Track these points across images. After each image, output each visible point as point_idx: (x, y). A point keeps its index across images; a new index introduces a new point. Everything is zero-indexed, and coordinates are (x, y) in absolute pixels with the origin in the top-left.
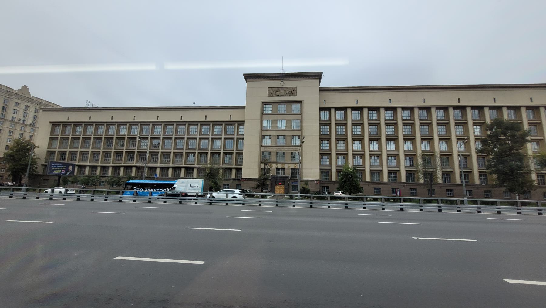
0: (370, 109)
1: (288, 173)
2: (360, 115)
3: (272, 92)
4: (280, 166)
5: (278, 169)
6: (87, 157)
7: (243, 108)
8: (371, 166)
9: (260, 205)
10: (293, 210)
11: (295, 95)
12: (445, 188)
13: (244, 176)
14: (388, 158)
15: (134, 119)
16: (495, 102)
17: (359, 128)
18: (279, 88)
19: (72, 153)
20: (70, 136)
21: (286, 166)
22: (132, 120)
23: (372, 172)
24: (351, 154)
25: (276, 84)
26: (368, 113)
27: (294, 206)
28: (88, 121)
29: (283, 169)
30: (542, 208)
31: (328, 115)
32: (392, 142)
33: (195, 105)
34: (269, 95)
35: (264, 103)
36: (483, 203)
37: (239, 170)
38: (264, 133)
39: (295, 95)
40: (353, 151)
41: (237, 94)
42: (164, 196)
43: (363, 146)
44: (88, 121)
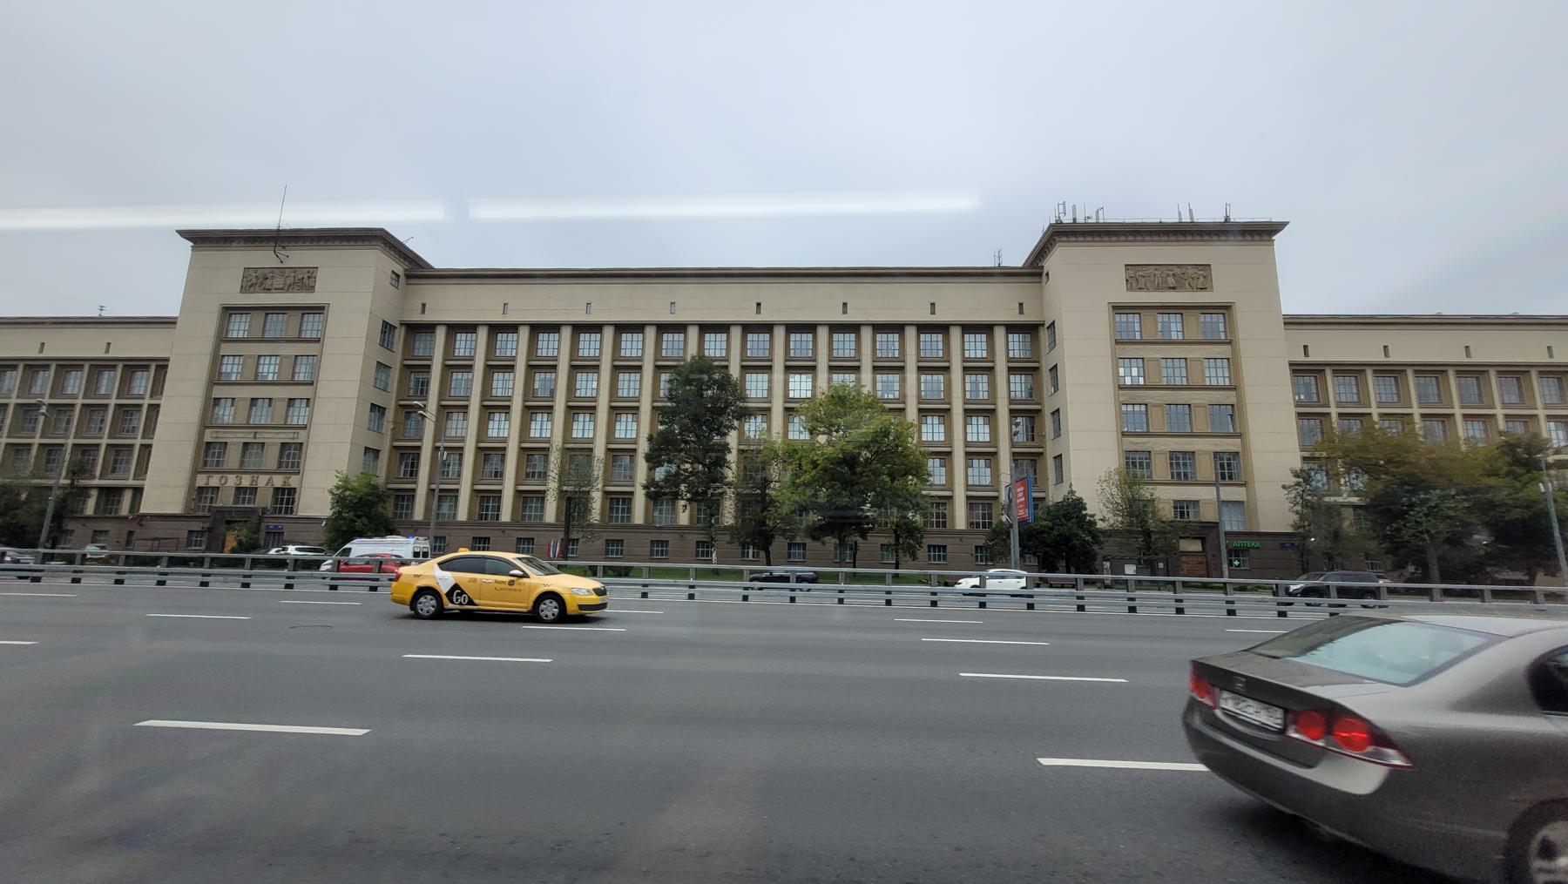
0: (968, 328)
1: (264, 500)
2: (984, 346)
3: (255, 280)
4: (246, 481)
5: (239, 490)
6: (128, 462)
7: (169, 322)
8: (968, 487)
9: (888, 602)
10: (839, 614)
11: (311, 289)
12: (693, 538)
13: (145, 508)
14: (968, 466)
15: (41, 351)
16: (845, 312)
17: (983, 379)
18: (267, 272)
19: (84, 452)
20: (113, 402)
21: (262, 481)
22: (32, 352)
23: (971, 502)
24: (962, 454)
25: (264, 258)
26: (874, 341)
27: (841, 601)
28: (37, 355)
29: (253, 490)
30: (127, 568)
31: (853, 345)
32: (981, 420)
33: (105, 314)
34: (1130, 288)
35: (229, 311)
36: (653, 573)
37: (138, 491)
38: (218, 392)
39: (311, 289)
40: (967, 444)
41: (159, 284)
42: (370, 570)
43: (949, 432)
44: (102, 355)
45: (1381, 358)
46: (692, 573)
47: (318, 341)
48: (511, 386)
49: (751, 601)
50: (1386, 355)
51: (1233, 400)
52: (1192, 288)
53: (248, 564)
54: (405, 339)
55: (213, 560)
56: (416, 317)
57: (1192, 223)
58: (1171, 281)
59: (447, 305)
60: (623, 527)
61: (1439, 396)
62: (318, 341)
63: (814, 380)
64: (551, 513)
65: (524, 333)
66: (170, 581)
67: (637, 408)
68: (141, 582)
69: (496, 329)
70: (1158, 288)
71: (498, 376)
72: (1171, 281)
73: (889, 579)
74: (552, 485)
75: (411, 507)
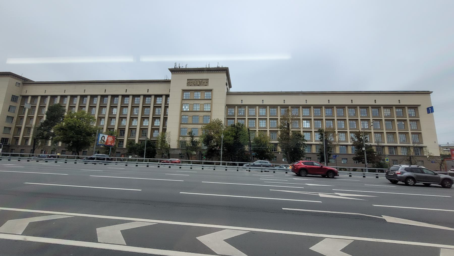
45: (398, 104)
46: (227, 164)
47: (211, 99)
48: (127, 112)
49: (171, 168)
50: (399, 102)
51: (210, 115)
52: (203, 85)
53: (215, 164)
54: (22, 100)
55: (379, 170)
56: (24, 94)
57: (186, 69)
58: (198, 83)
59: (32, 91)
60: (121, 149)
61: (403, 114)
62: (211, 99)
63: (117, 110)
64: (29, 143)
65: (131, 97)
66: (161, 166)
67: (137, 117)
68: (90, 164)
69: (145, 96)
70: (195, 85)
71: (157, 109)
72: (198, 83)
73: (377, 171)
74: (31, 136)
75: (123, 144)
